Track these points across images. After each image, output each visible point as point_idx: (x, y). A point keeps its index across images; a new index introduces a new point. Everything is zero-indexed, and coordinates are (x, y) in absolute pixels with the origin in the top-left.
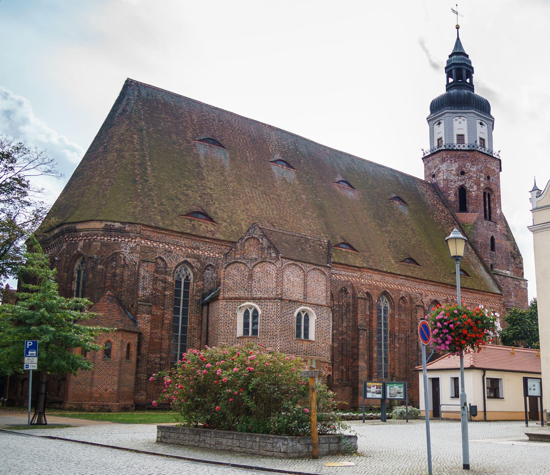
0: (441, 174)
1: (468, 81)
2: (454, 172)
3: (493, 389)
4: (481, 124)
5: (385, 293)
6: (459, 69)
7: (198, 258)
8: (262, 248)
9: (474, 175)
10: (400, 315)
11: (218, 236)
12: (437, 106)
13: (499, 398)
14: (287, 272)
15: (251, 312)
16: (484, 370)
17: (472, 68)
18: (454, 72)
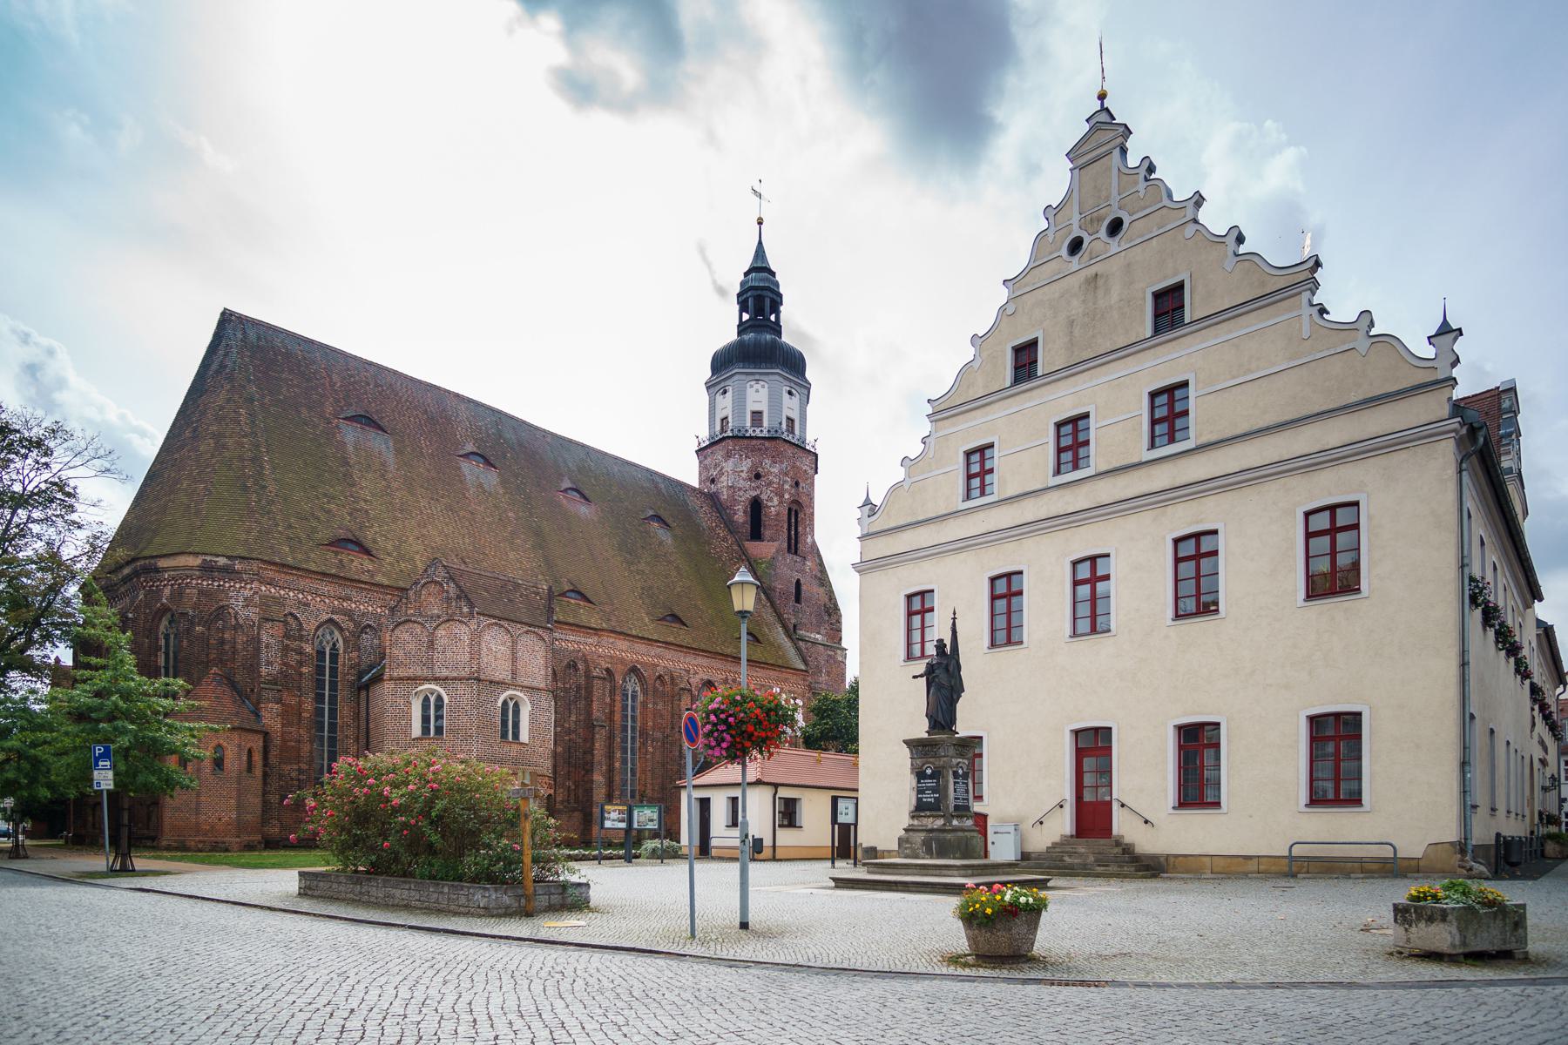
0: (724, 478)
1: (773, 318)
2: (744, 475)
3: (788, 814)
4: (790, 393)
5: (633, 670)
6: (760, 297)
7: (349, 614)
8: (448, 598)
11: (379, 579)
12: (723, 362)
15: (432, 699)
16: (776, 786)
17: (780, 296)
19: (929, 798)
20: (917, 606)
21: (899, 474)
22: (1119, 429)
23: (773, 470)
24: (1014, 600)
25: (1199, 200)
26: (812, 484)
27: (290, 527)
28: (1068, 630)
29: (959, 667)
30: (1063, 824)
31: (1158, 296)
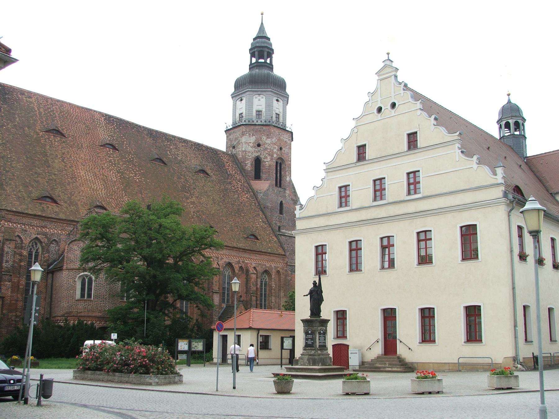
0: (240, 146)
1: (268, 61)
4: (277, 100)
6: (262, 50)
7: (45, 234)
9: (269, 147)
11: (62, 216)
13: (268, 349)
16: (258, 330)
17: (273, 50)
18: (256, 53)
19: (310, 342)
21: (312, 193)
22: (396, 187)
23: (267, 141)
24: (359, 251)
26: (290, 148)
27: (20, 191)
29: (322, 292)
30: (379, 350)
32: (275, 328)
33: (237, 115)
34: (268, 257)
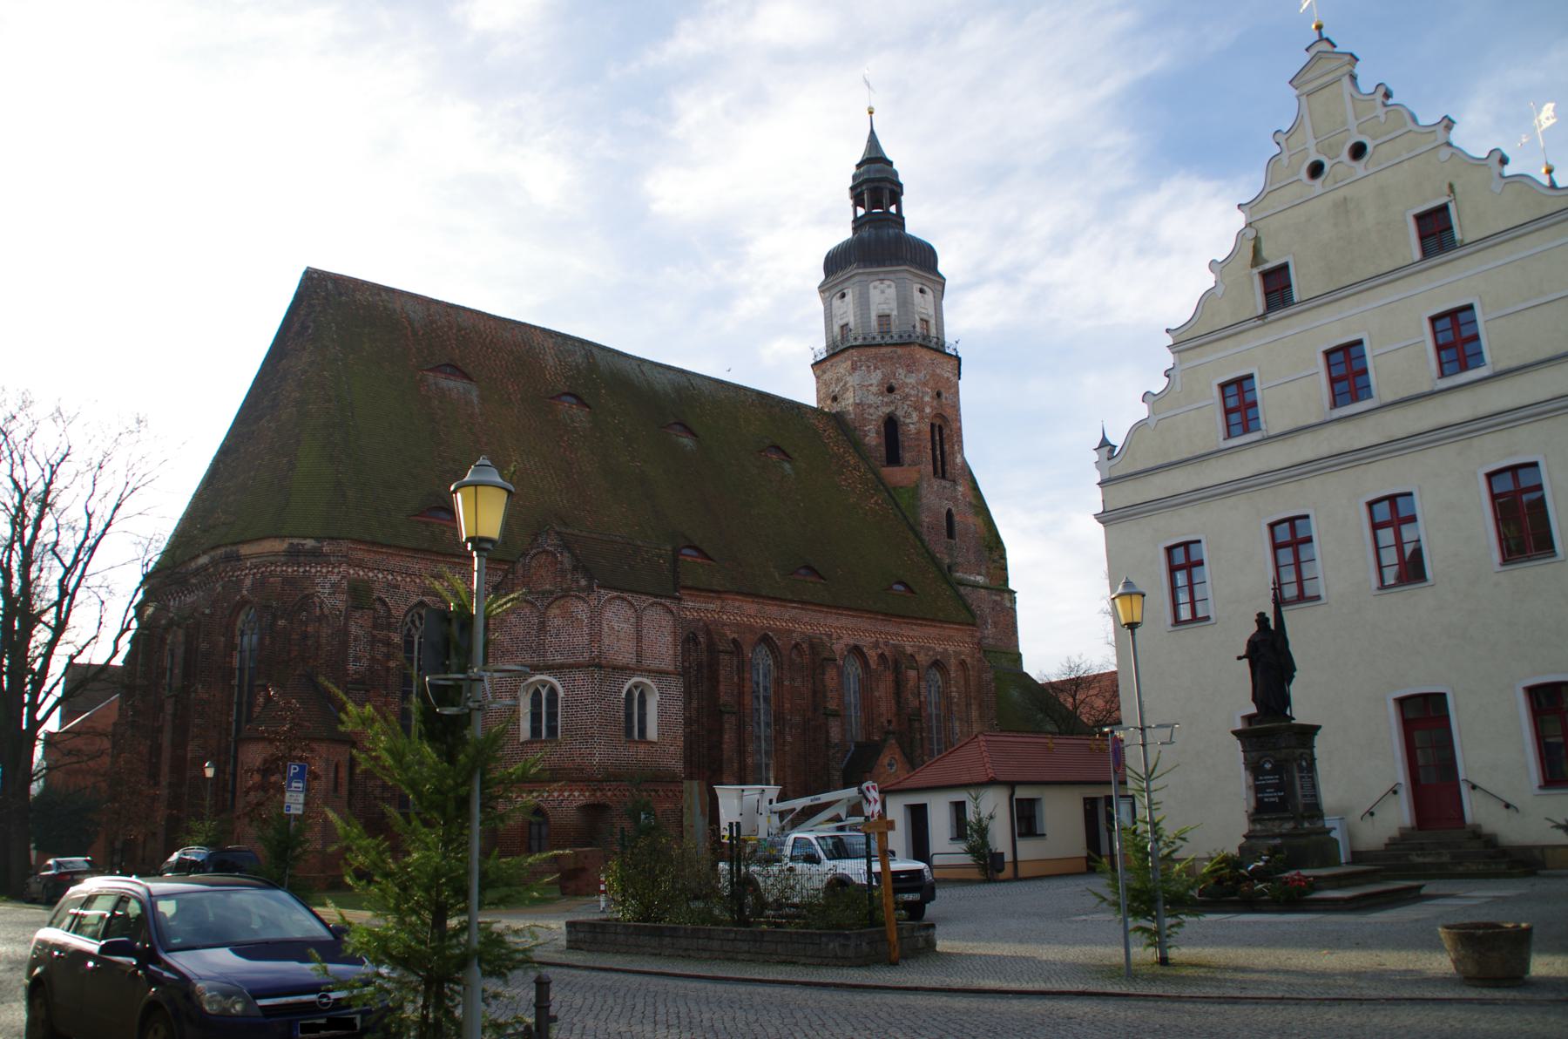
0: (850, 394)
2: (874, 389)
3: (1026, 821)
4: (922, 291)
5: (765, 639)
6: (876, 185)
8: (562, 570)
10: (792, 679)
12: (836, 262)
14: (608, 614)
15: (544, 693)
17: (900, 186)
19: (1271, 797)
20: (1179, 557)
21: (1143, 412)
23: (908, 380)
25: (1448, 123)
28: (1375, 581)
30: (1399, 815)
31: (1420, 218)
32: (1047, 779)
33: (836, 329)
34: (937, 631)
